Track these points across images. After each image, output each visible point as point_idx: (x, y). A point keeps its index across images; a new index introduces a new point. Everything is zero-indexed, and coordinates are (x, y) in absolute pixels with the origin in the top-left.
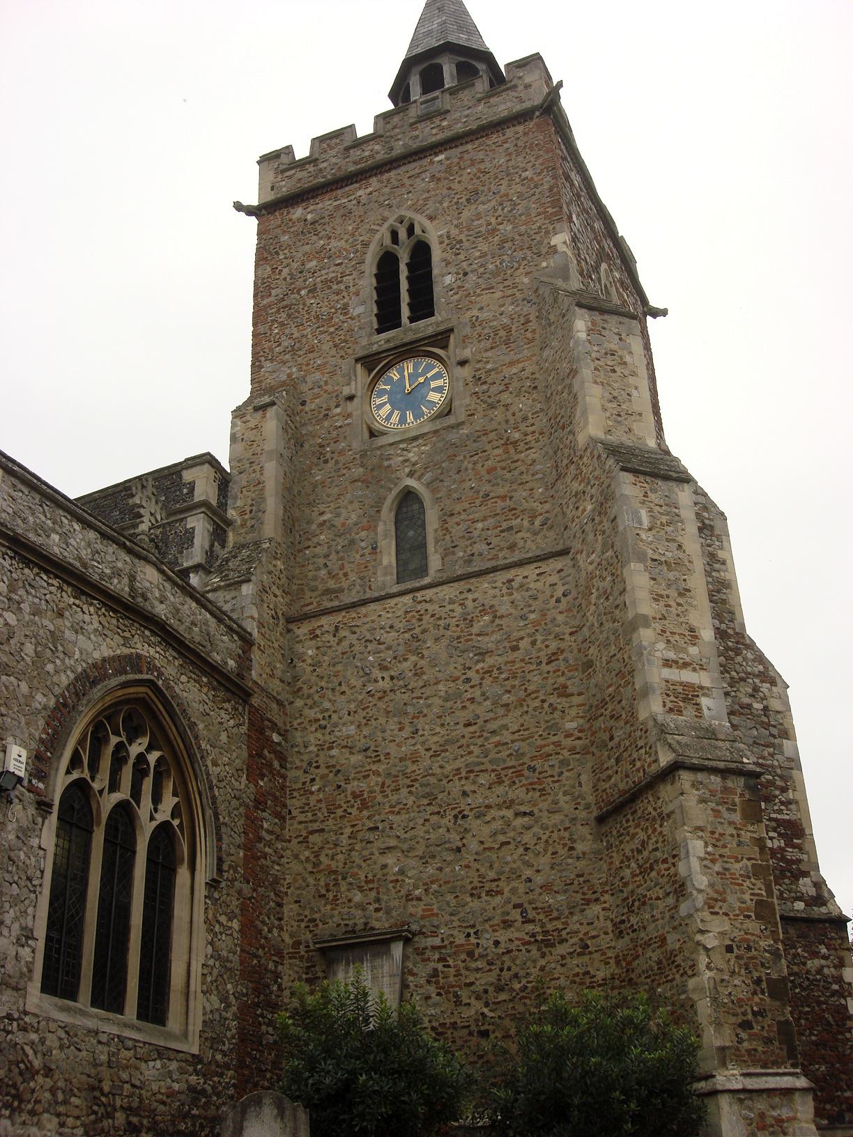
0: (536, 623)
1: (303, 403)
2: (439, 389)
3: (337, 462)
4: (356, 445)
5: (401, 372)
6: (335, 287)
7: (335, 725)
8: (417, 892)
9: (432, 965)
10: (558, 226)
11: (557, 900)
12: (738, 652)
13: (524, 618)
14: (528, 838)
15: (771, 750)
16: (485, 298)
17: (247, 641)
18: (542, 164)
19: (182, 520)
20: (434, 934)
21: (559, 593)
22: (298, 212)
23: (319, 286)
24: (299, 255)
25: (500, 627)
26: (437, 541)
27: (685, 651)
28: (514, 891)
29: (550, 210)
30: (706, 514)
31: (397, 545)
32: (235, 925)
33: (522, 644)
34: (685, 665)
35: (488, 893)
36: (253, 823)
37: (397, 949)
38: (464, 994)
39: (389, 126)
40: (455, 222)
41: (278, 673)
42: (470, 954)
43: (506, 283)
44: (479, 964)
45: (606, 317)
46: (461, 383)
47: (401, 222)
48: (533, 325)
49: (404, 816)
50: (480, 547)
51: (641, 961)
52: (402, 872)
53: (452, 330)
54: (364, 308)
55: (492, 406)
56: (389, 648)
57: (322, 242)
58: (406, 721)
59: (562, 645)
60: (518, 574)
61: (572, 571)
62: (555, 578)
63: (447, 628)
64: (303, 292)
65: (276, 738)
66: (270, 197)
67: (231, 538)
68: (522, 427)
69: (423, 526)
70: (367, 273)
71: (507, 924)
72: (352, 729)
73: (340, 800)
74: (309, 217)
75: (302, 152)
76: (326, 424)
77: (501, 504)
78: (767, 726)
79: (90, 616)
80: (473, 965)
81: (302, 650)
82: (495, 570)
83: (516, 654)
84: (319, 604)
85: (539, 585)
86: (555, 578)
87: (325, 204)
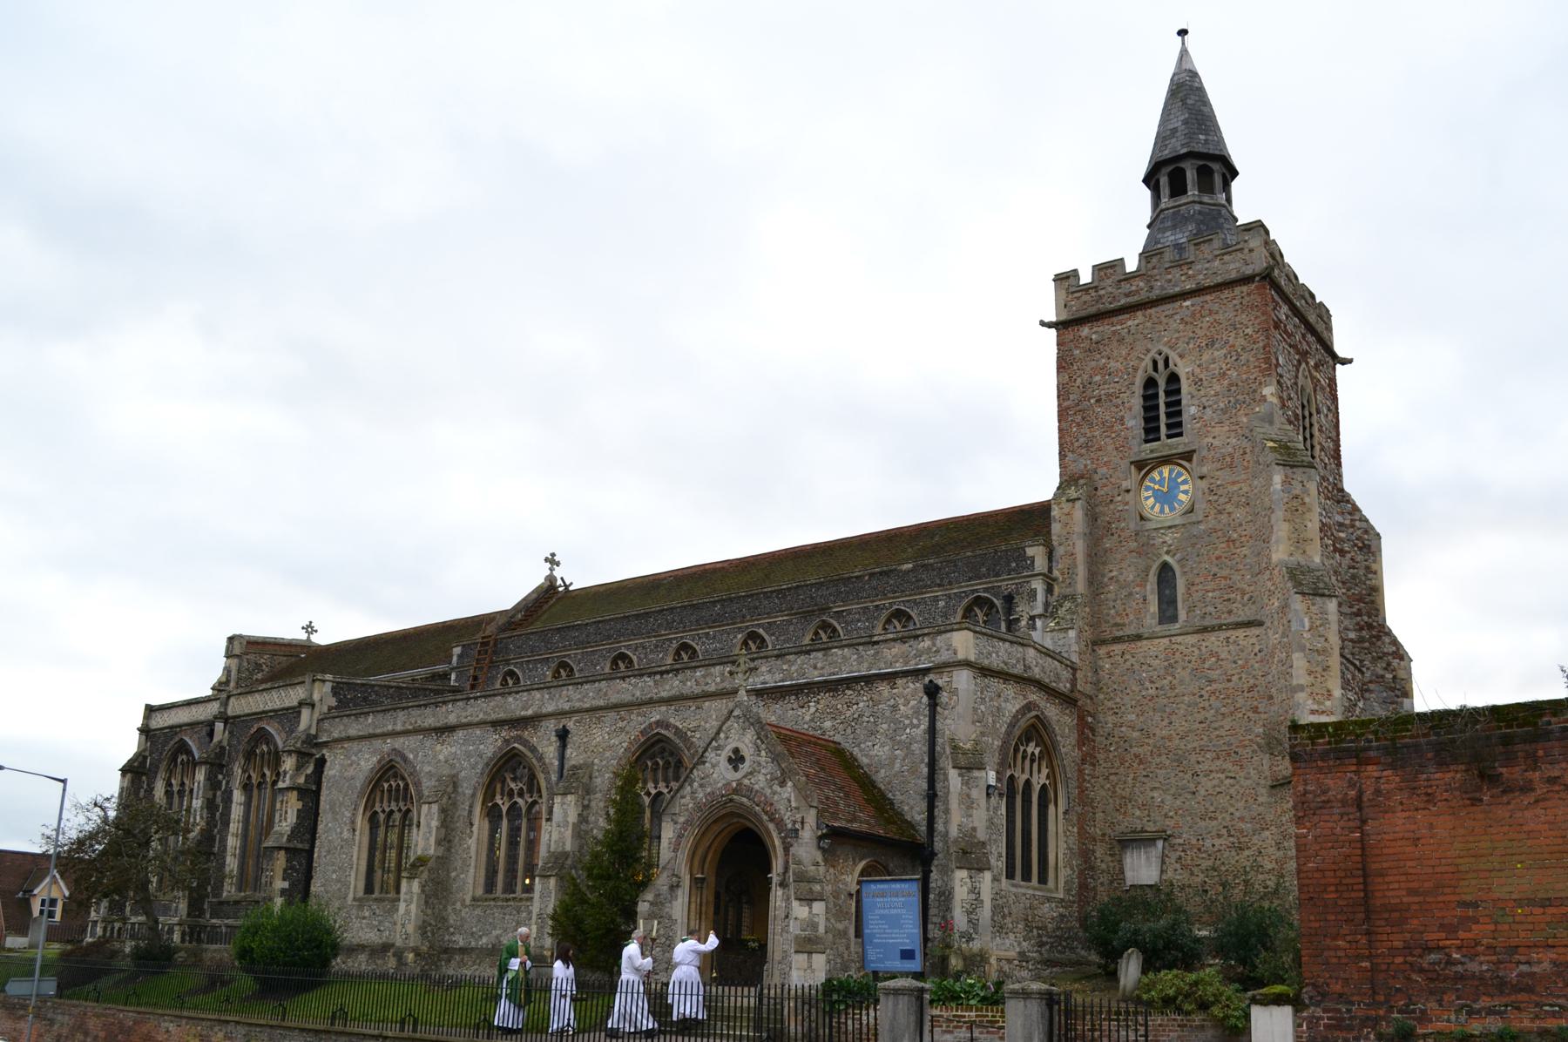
0: (1243, 667)
1: (1096, 489)
2: (1185, 492)
3: (1119, 536)
4: (1132, 526)
5: (1161, 474)
6: (1114, 401)
7: (1124, 713)
8: (1171, 814)
9: (1178, 853)
10: (1268, 379)
11: (1247, 827)
12: (1378, 638)
13: (1235, 662)
14: (1232, 791)
15: (1394, 706)
16: (1217, 430)
17: (1074, 669)
18: (1259, 324)
19: (1028, 582)
20: (1180, 837)
21: (1256, 650)
22: (1085, 331)
23: (1103, 397)
24: (1088, 369)
25: (1221, 667)
26: (1184, 601)
27: (1323, 704)
28: (1223, 819)
29: (1264, 366)
30: (1366, 537)
31: (1159, 599)
32: (1075, 830)
33: (1234, 678)
34: (1323, 712)
35: (1210, 818)
36: (1081, 771)
37: (1160, 844)
38: (1196, 870)
39: (1150, 266)
40: (1198, 363)
41: (1089, 679)
42: (1199, 850)
43: (1232, 420)
44: (1204, 855)
45: (1295, 470)
46: (1200, 493)
47: (1160, 354)
48: (1247, 457)
49: (1163, 771)
50: (1210, 609)
51: (1288, 865)
52: (1162, 802)
53: (1194, 451)
55: (1220, 512)
56: (1155, 670)
57: (1104, 361)
58: (1165, 715)
59: (1257, 682)
60: (1233, 634)
61: (1265, 637)
62: (1254, 640)
63: (1190, 662)
64: (1092, 401)
65: (1090, 719)
66: (1064, 317)
67: (1056, 589)
68: (1239, 530)
69: (1175, 587)
70: (1137, 394)
71: (1219, 836)
72: (1133, 717)
73: (1128, 757)
74: (1094, 337)
75: (1086, 277)
76: (1112, 507)
77: (1223, 582)
78: (1393, 689)
79: (1010, 690)
80: (1201, 856)
81: (1102, 664)
82: (1220, 628)
83: (1230, 684)
84: (1111, 633)
85: (1245, 643)
86: (1254, 640)
87: (1104, 328)
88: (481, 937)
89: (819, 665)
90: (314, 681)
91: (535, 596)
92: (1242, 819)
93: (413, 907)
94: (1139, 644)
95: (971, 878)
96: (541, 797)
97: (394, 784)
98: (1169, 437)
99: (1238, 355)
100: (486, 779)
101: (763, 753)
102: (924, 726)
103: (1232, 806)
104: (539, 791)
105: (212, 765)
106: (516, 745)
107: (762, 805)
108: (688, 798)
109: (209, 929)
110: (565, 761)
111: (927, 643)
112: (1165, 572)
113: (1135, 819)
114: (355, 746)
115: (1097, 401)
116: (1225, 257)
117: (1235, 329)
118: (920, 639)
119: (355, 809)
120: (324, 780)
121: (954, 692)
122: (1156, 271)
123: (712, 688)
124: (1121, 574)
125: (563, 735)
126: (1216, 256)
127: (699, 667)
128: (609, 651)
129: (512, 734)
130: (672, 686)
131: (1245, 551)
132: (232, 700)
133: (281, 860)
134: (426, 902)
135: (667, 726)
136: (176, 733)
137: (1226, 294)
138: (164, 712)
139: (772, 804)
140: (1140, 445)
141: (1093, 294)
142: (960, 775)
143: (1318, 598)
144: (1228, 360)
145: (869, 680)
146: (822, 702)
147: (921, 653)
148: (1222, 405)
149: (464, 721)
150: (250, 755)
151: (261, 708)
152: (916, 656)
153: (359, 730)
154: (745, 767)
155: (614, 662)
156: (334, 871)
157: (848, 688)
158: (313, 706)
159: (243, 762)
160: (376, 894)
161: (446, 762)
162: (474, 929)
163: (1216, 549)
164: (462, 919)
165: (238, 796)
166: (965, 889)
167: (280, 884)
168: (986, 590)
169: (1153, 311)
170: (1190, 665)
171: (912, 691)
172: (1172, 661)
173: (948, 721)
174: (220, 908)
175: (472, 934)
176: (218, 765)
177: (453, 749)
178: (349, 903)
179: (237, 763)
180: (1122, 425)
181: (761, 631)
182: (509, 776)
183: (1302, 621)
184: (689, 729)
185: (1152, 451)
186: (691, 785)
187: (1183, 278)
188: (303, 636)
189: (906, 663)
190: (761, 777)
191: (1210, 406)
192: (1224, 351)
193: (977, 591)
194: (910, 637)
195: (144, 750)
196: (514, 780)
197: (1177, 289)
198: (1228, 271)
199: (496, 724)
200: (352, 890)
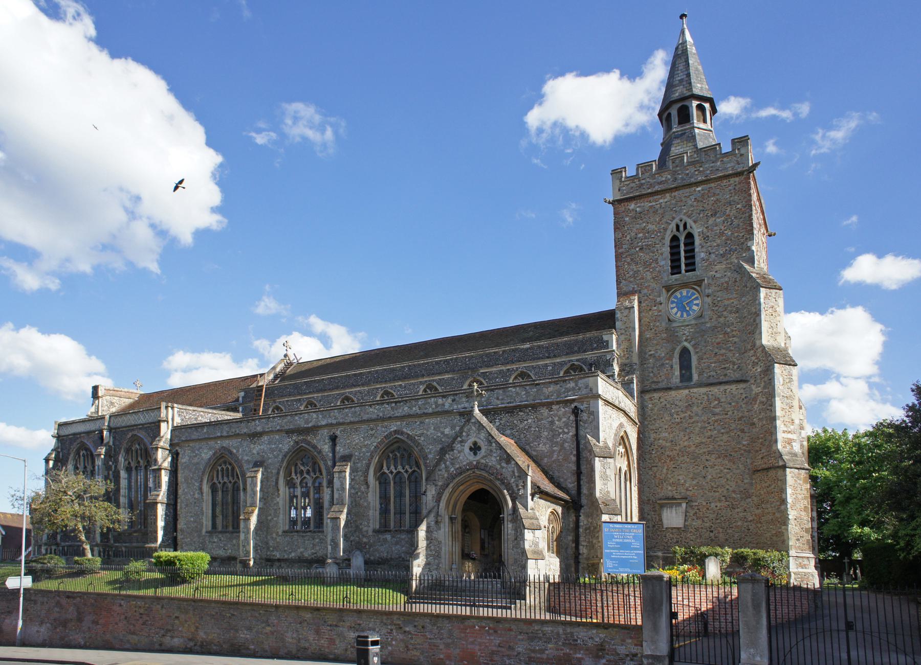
0: (734, 406)
2: (697, 305)
3: (655, 330)
7: (661, 432)
8: (690, 489)
13: (730, 404)
14: (728, 476)
20: (696, 502)
22: (632, 206)
23: (644, 247)
34: (789, 432)
35: (714, 491)
40: (706, 226)
43: (728, 262)
49: (685, 465)
50: (713, 373)
54: (665, 263)
55: (719, 317)
56: (680, 408)
58: (687, 434)
62: (742, 391)
64: (637, 249)
71: (720, 501)
74: (638, 209)
77: (721, 358)
80: (709, 512)
83: (727, 416)
86: (742, 391)
87: (646, 204)
88: (291, 553)
89: (500, 397)
92: (734, 491)
96: (321, 474)
97: (225, 468)
98: (687, 271)
102: (572, 432)
104: (320, 471)
106: (303, 445)
108: (444, 471)
110: (336, 454)
111: (572, 384)
112: (685, 353)
113: (668, 491)
114: (197, 445)
115: (640, 249)
117: (730, 205)
120: (179, 464)
122: (678, 168)
123: (430, 410)
125: (334, 439)
127: (420, 398)
129: (299, 438)
135: (402, 433)
136: (78, 438)
140: (668, 276)
141: (637, 183)
143: (787, 366)
144: (725, 224)
145: (534, 407)
146: (504, 419)
148: (722, 252)
149: (267, 430)
150: (128, 451)
152: (564, 392)
154: (483, 452)
155: (343, 402)
156: (192, 516)
159: (124, 454)
161: (258, 454)
162: (286, 549)
164: (277, 542)
165: (123, 474)
169: (676, 193)
170: (702, 406)
171: (562, 415)
172: (690, 403)
175: (285, 551)
177: (262, 447)
178: (204, 533)
179: (121, 455)
180: (657, 263)
181: (435, 384)
182: (299, 463)
184: (416, 435)
185: (676, 280)
186: (445, 463)
187: (697, 173)
190: (493, 459)
191: (713, 253)
192: (723, 218)
193: (572, 361)
195: (58, 448)
196: (303, 464)
199: (289, 432)
200: (204, 526)
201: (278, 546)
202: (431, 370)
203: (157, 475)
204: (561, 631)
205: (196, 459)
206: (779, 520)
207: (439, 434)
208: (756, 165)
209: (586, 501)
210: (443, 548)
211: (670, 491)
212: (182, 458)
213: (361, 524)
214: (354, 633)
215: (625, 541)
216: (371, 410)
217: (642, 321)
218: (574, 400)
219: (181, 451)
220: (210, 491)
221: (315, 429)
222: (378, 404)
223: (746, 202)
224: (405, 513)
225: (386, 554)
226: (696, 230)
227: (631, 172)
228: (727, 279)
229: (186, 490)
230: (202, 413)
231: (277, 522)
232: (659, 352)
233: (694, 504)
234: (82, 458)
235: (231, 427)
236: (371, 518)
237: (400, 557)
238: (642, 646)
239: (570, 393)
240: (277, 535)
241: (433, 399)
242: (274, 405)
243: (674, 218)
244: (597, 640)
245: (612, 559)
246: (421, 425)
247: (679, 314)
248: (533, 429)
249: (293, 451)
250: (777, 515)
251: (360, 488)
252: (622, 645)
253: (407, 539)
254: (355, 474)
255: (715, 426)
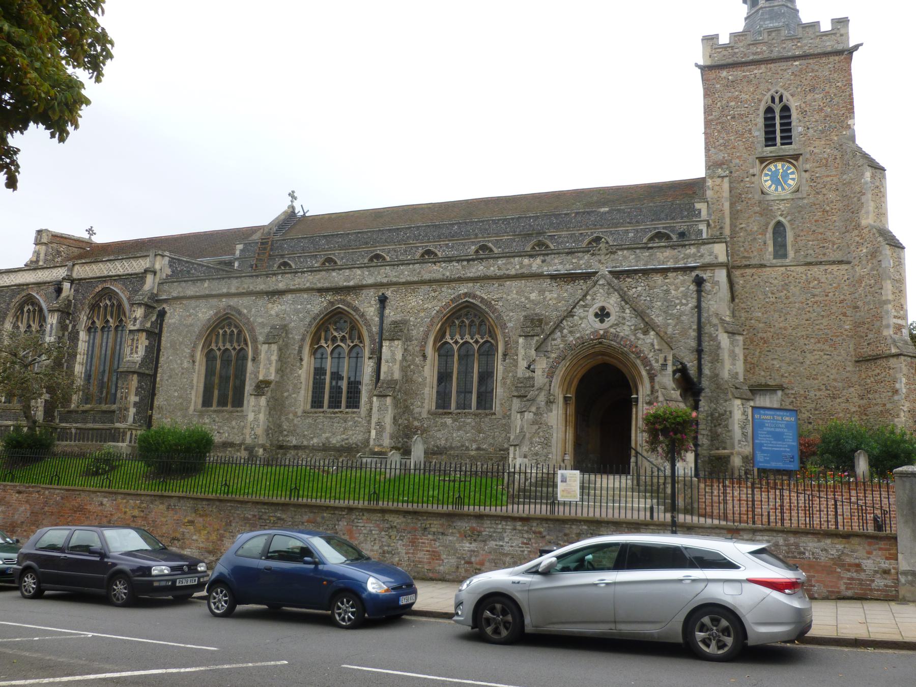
0: (836, 288)
2: (793, 179)
3: (747, 203)
4: (757, 197)
5: (776, 166)
6: (745, 119)
13: (831, 285)
14: (828, 362)
16: (817, 143)
20: (792, 389)
22: (724, 73)
23: (737, 116)
28: (823, 379)
34: (899, 318)
37: (780, 393)
42: (806, 397)
48: (838, 161)
49: (781, 348)
50: (811, 252)
52: (780, 367)
53: (801, 154)
54: (759, 133)
55: (818, 193)
59: (846, 298)
60: (830, 268)
63: (799, 283)
64: (729, 117)
66: (709, 63)
68: (831, 205)
71: (820, 390)
72: (760, 314)
73: (755, 339)
74: (730, 78)
82: (821, 263)
83: (827, 298)
86: (844, 272)
87: (739, 73)
88: (312, 438)
90: (156, 255)
91: (283, 217)
92: (835, 380)
93: (262, 417)
94: (764, 270)
95: (743, 405)
97: (228, 331)
98: (782, 144)
99: (832, 99)
100: (313, 329)
101: (628, 311)
102: (693, 303)
103: (829, 372)
105: (62, 312)
107: (628, 347)
108: (559, 340)
109: (59, 430)
111: (693, 250)
114: (193, 303)
115: (732, 118)
116: (824, 38)
118: (687, 247)
119: (194, 347)
120: (164, 326)
121: (717, 283)
122: (774, 41)
123: (513, 272)
124: (748, 226)
125: (383, 300)
126: (817, 36)
128: (367, 252)
129: (336, 298)
130: (478, 269)
131: (835, 218)
132: (77, 267)
133: (134, 381)
134: (269, 413)
135: (475, 297)
137: (824, 60)
138: (10, 274)
139: (637, 347)
140: (762, 147)
141: (730, 51)
142: (729, 337)
144: (824, 101)
145: (646, 272)
147: (690, 256)
148: (820, 128)
149: (292, 287)
150: (94, 307)
151: (106, 273)
152: (683, 258)
153: (197, 292)
154: (612, 319)
156: (175, 391)
157: (628, 277)
158: (155, 273)
159: (88, 312)
160: (214, 407)
162: (306, 433)
163: (815, 215)
164: (295, 425)
165: (83, 336)
166: (740, 412)
167: (133, 398)
168: (664, 228)
169: (772, 65)
170: (800, 285)
171: (681, 286)
172: (787, 282)
173: (711, 302)
174: (68, 416)
175: (304, 435)
176: (66, 313)
177: (283, 307)
178: (191, 412)
179: (83, 313)
180: (751, 134)
181: (490, 245)
183: (889, 261)
184: (493, 300)
185: (771, 152)
186: (561, 332)
187: (794, 47)
188: (86, 236)
189: (676, 263)
190: (626, 328)
191: (812, 128)
192: (822, 95)
193: (658, 228)
194: (678, 246)
197: (790, 54)
198: (825, 47)
199: (321, 291)
200: (193, 404)
201: (295, 431)
202: (487, 230)
203: (136, 338)
204: (781, 542)
205: (190, 319)
206: (891, 412)
207: (523, 300)
208: (856, 47)
209: (707, 383)
210: (555, 435)
211: (763, 376)
212: (170, 318)
213: (412, 404)
214: (471, 543)
215: (777, 430)
216: (435, 268)
217: (733, 192)
218: (694, 268)
219: (170, 310)
220: (205, 360)
221: (357, 289)
222: (444, 262)
223: (846, 81)
224: (471, 392)
225: (444, 442)
226: (794, 104)
227: (724, 40)
228: (826, 156)
229: (171, 358)
230: (195, 266)
231: (295, 399)
232: (751, 226)
233: (791, 392)
234: (26, 315)
235: (242, 282)
236: (426, 396)
237: (463, 446)
238: (897, 560)
239: (689, 260)
240: (294, 416)
241: (517, 259)
242: (282, 261)
243: (769, 90)
244: (833, 552)
245: (763, 451)
246: (500, 287)
247: (773, 187)
248: (642, 298)
249: (325, 313)
250: (889, 406)
251: (414, 360)
252: (869, 558)
253: (473, 424)
254: (409, 343)
255: (815, 308)
